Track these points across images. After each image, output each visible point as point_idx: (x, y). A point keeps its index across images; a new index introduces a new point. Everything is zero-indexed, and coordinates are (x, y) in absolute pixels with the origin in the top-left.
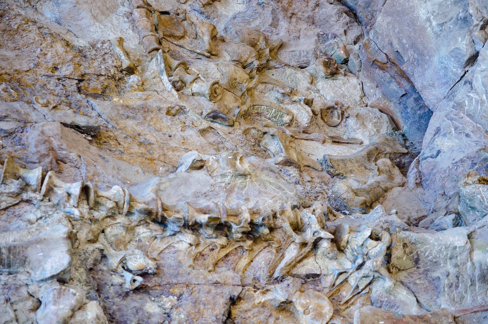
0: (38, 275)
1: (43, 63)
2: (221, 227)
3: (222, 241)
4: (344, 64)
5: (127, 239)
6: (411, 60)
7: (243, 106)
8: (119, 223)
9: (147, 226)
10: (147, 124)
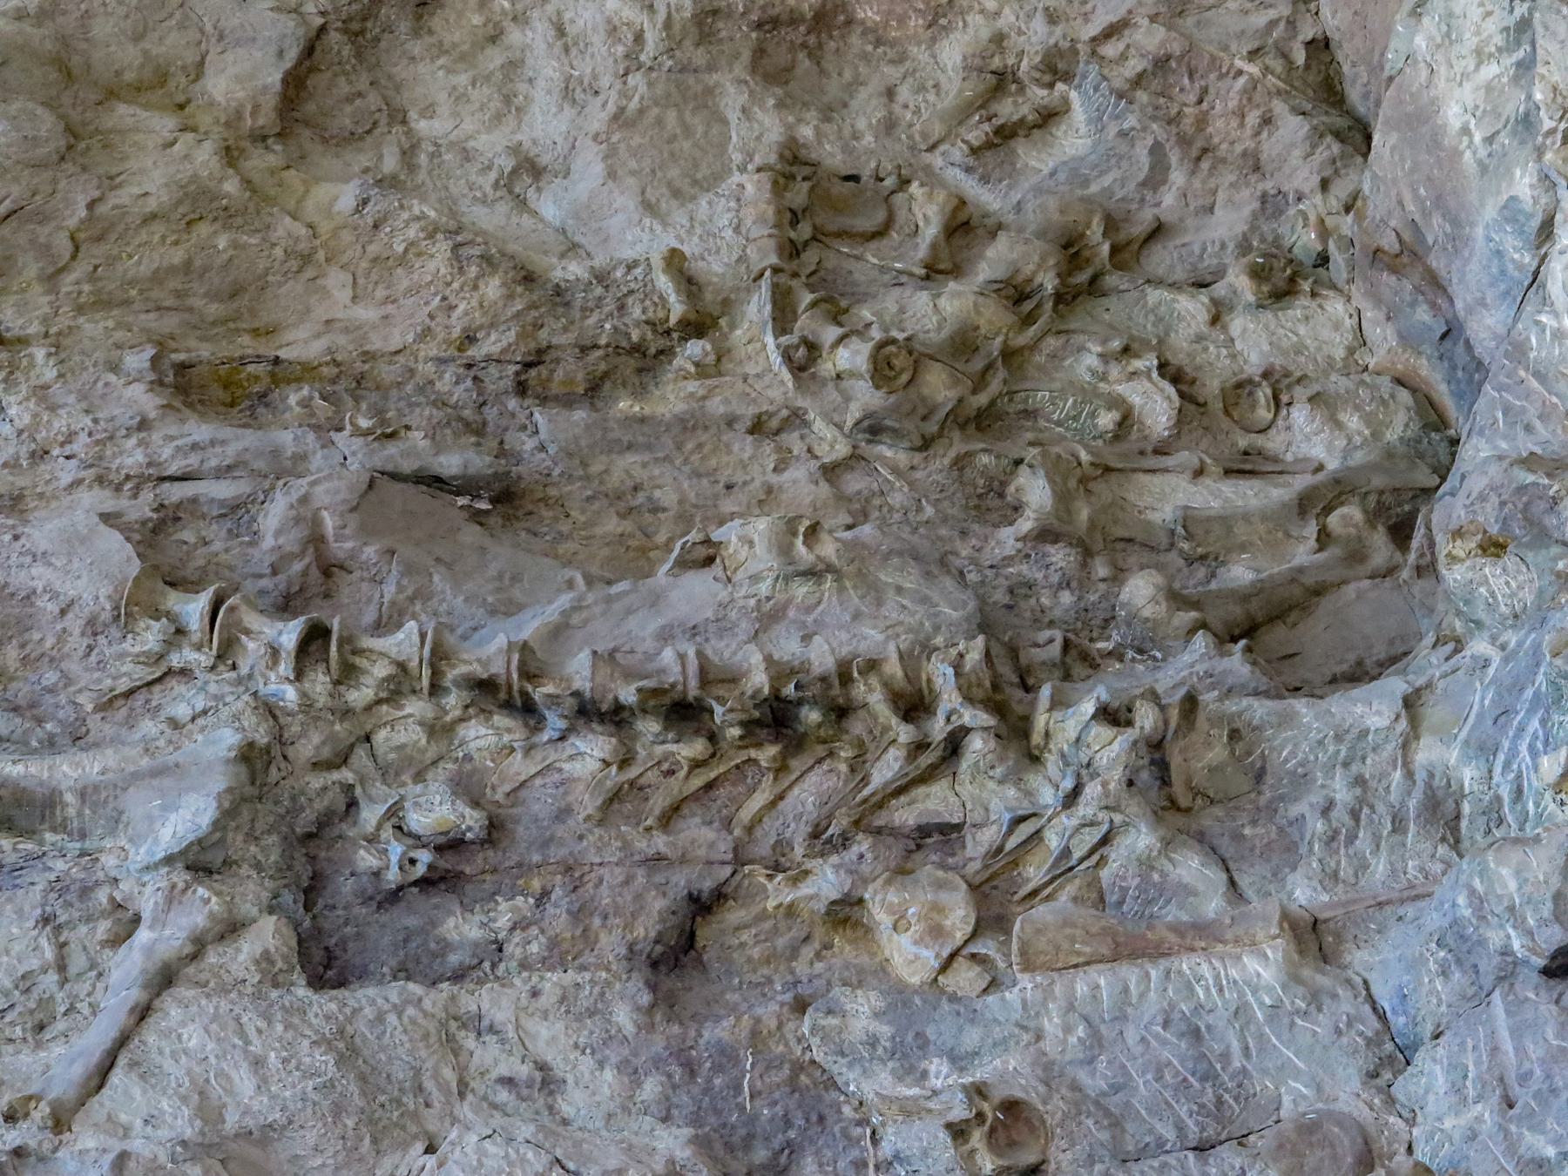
2: (683, 712)
5: (430, 755)
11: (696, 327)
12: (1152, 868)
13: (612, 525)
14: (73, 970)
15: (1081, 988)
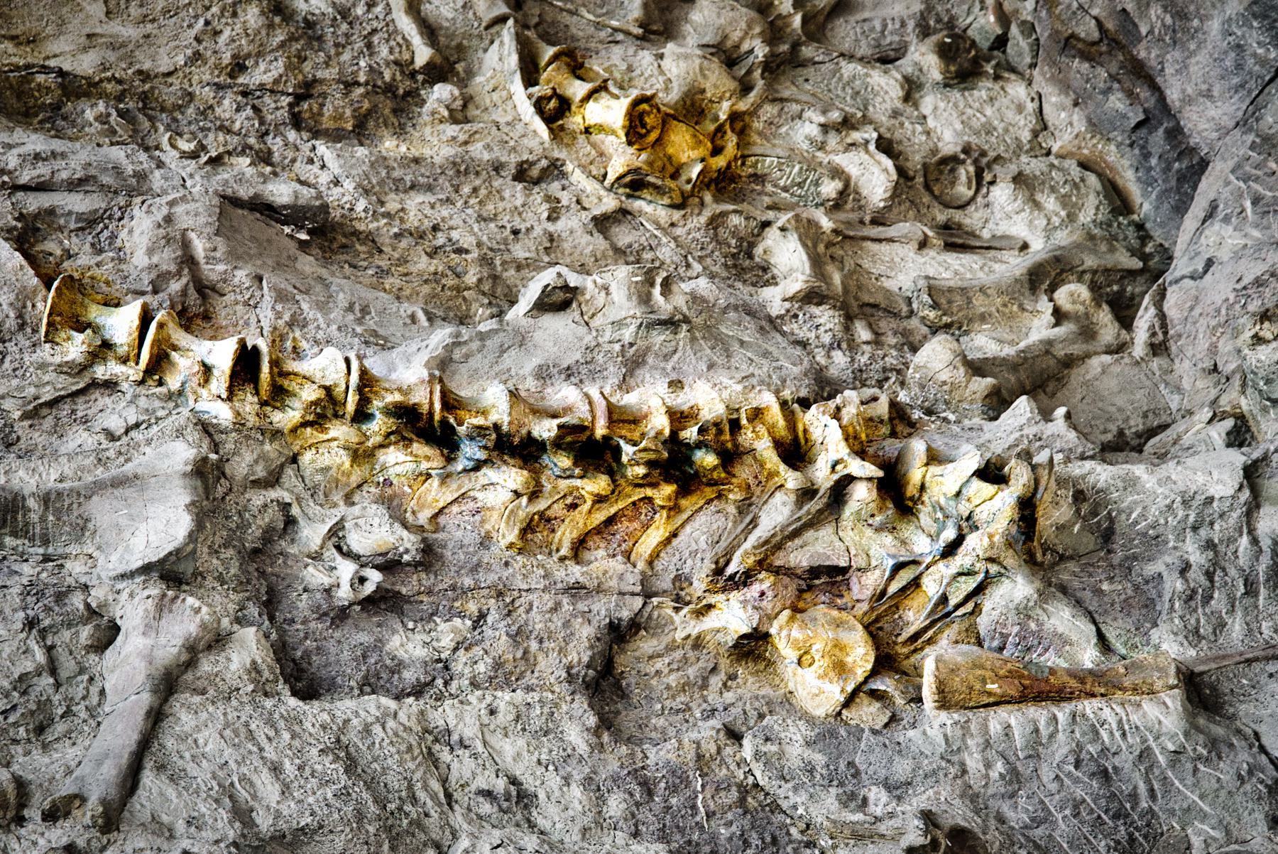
0: (113, 563)
1: (209, 53)
2: (593, 452)
3: (599, 484)
4: (998, 49)
5: (355, 479)
6: (1157, 31)
7: (716, 159)
8: (335, 439)
9: (406, 447)
10: (459, 204)
11: (438, 72)
12: (1029, 617)
13: (422, 264)
14: (63, 674)
15: (995, 727)
